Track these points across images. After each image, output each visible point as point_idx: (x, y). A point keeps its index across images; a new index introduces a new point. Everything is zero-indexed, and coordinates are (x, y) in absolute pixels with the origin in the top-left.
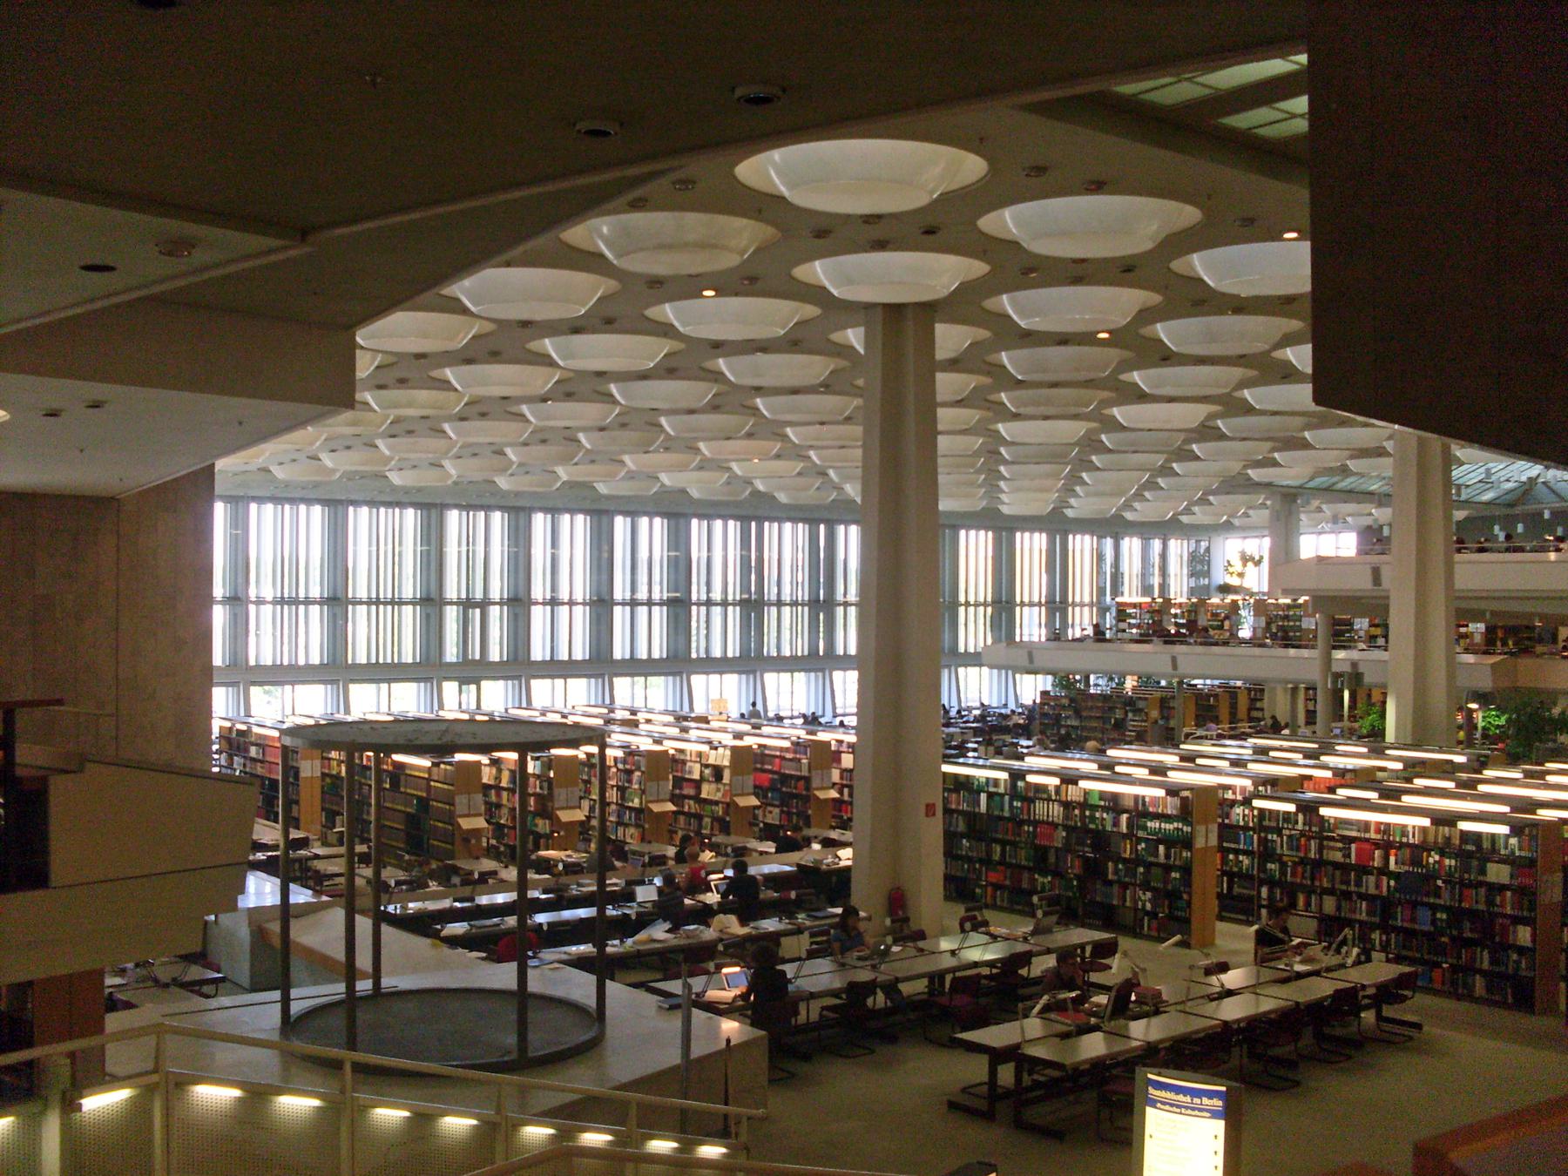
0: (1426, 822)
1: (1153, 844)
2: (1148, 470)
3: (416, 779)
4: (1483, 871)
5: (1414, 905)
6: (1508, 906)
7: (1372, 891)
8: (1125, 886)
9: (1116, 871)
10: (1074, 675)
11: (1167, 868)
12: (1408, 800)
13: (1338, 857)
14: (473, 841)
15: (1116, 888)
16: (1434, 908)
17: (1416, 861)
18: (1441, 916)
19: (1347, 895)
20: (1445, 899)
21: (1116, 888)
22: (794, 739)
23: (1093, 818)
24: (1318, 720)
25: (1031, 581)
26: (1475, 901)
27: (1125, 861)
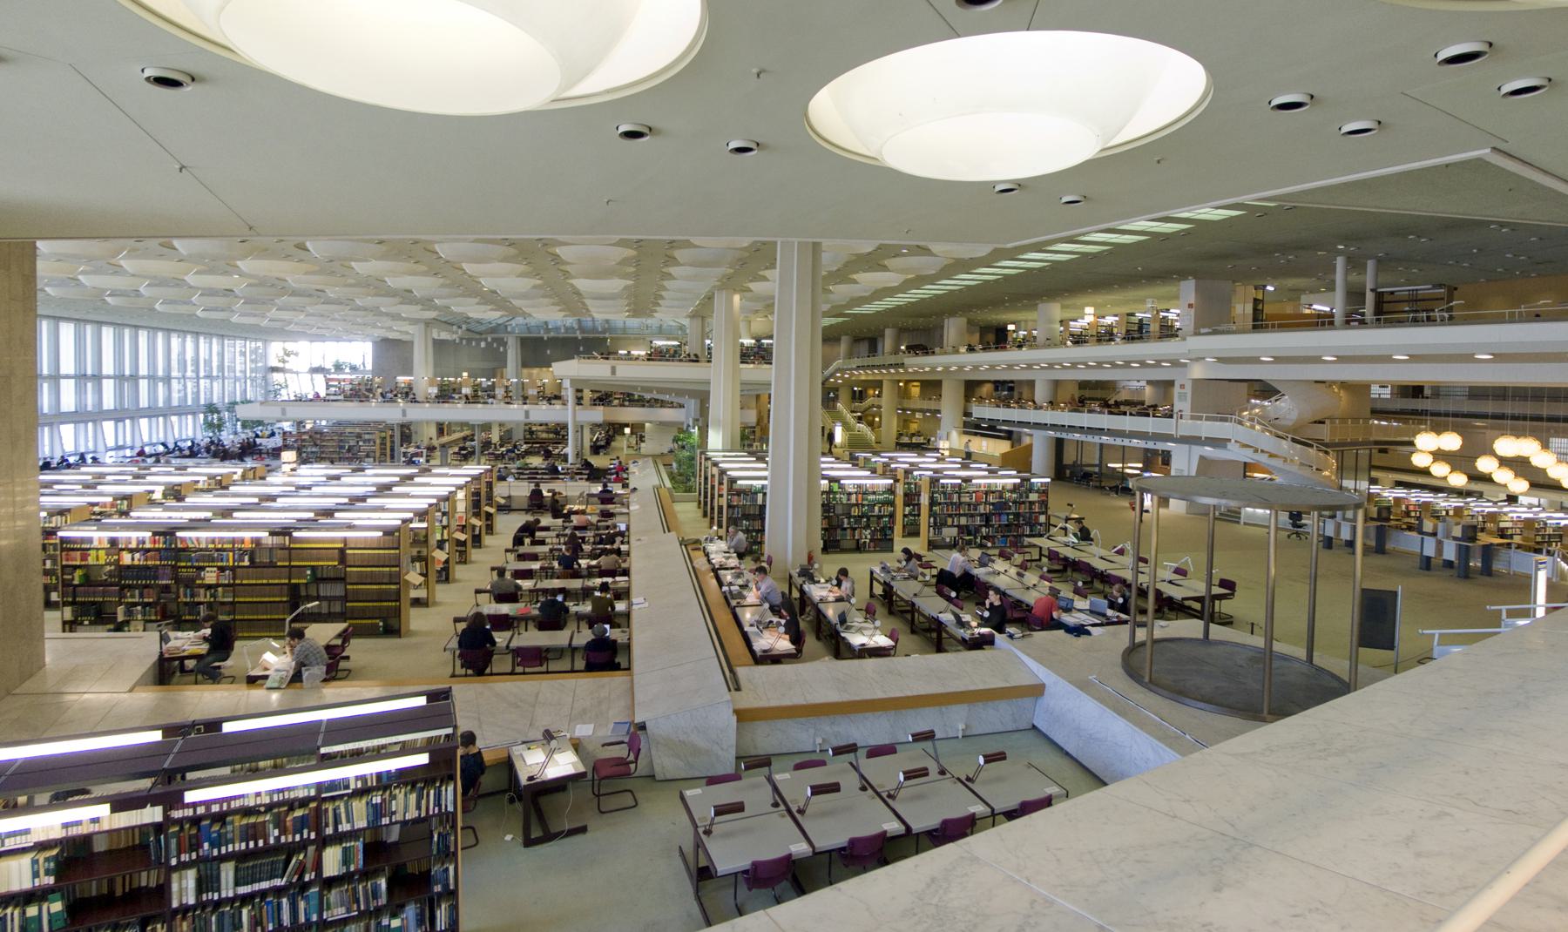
0: (959, 481)
1: (872, 506)
2: (146, 277)
3: (301, 551)
4: (1027, 497)
5: (1000, 515)
6: (1036, 508)
7: (982, 511)
8: (855, 529)
9: (849, 523)
10: (321, 420)
11: (880, 517)
12: (149, 478)
13: (967, 500)
14: (1080, 584)
15: (849, 531)
16: (1008, 514)
17: (1001, 497)
18: (1011, 517)
19: (972, 516)
20: (1013, 510)
21: (849, 531)
22: (280, 474)
23: (835, 499)
24: (570, 441)
25: (190, 354)
26: (1023, 509)
27: (855, 517)
